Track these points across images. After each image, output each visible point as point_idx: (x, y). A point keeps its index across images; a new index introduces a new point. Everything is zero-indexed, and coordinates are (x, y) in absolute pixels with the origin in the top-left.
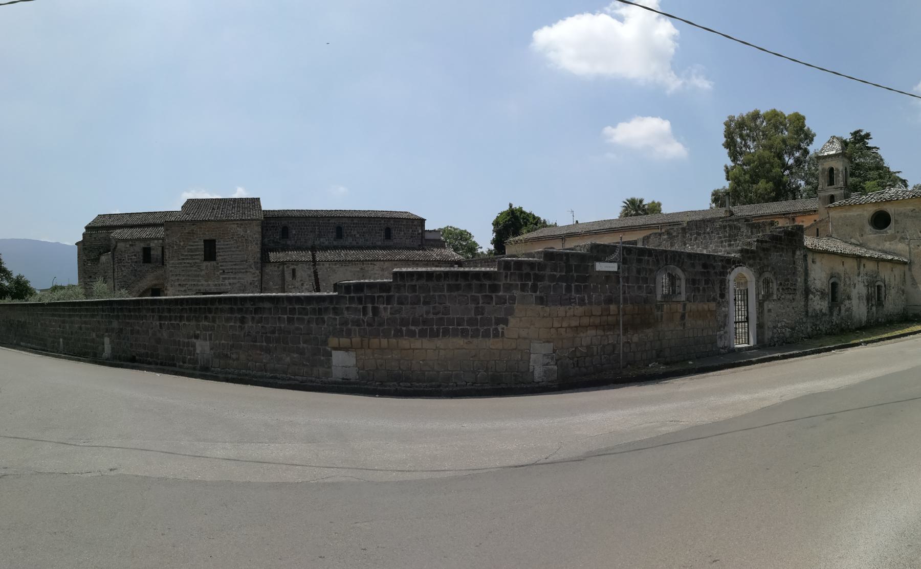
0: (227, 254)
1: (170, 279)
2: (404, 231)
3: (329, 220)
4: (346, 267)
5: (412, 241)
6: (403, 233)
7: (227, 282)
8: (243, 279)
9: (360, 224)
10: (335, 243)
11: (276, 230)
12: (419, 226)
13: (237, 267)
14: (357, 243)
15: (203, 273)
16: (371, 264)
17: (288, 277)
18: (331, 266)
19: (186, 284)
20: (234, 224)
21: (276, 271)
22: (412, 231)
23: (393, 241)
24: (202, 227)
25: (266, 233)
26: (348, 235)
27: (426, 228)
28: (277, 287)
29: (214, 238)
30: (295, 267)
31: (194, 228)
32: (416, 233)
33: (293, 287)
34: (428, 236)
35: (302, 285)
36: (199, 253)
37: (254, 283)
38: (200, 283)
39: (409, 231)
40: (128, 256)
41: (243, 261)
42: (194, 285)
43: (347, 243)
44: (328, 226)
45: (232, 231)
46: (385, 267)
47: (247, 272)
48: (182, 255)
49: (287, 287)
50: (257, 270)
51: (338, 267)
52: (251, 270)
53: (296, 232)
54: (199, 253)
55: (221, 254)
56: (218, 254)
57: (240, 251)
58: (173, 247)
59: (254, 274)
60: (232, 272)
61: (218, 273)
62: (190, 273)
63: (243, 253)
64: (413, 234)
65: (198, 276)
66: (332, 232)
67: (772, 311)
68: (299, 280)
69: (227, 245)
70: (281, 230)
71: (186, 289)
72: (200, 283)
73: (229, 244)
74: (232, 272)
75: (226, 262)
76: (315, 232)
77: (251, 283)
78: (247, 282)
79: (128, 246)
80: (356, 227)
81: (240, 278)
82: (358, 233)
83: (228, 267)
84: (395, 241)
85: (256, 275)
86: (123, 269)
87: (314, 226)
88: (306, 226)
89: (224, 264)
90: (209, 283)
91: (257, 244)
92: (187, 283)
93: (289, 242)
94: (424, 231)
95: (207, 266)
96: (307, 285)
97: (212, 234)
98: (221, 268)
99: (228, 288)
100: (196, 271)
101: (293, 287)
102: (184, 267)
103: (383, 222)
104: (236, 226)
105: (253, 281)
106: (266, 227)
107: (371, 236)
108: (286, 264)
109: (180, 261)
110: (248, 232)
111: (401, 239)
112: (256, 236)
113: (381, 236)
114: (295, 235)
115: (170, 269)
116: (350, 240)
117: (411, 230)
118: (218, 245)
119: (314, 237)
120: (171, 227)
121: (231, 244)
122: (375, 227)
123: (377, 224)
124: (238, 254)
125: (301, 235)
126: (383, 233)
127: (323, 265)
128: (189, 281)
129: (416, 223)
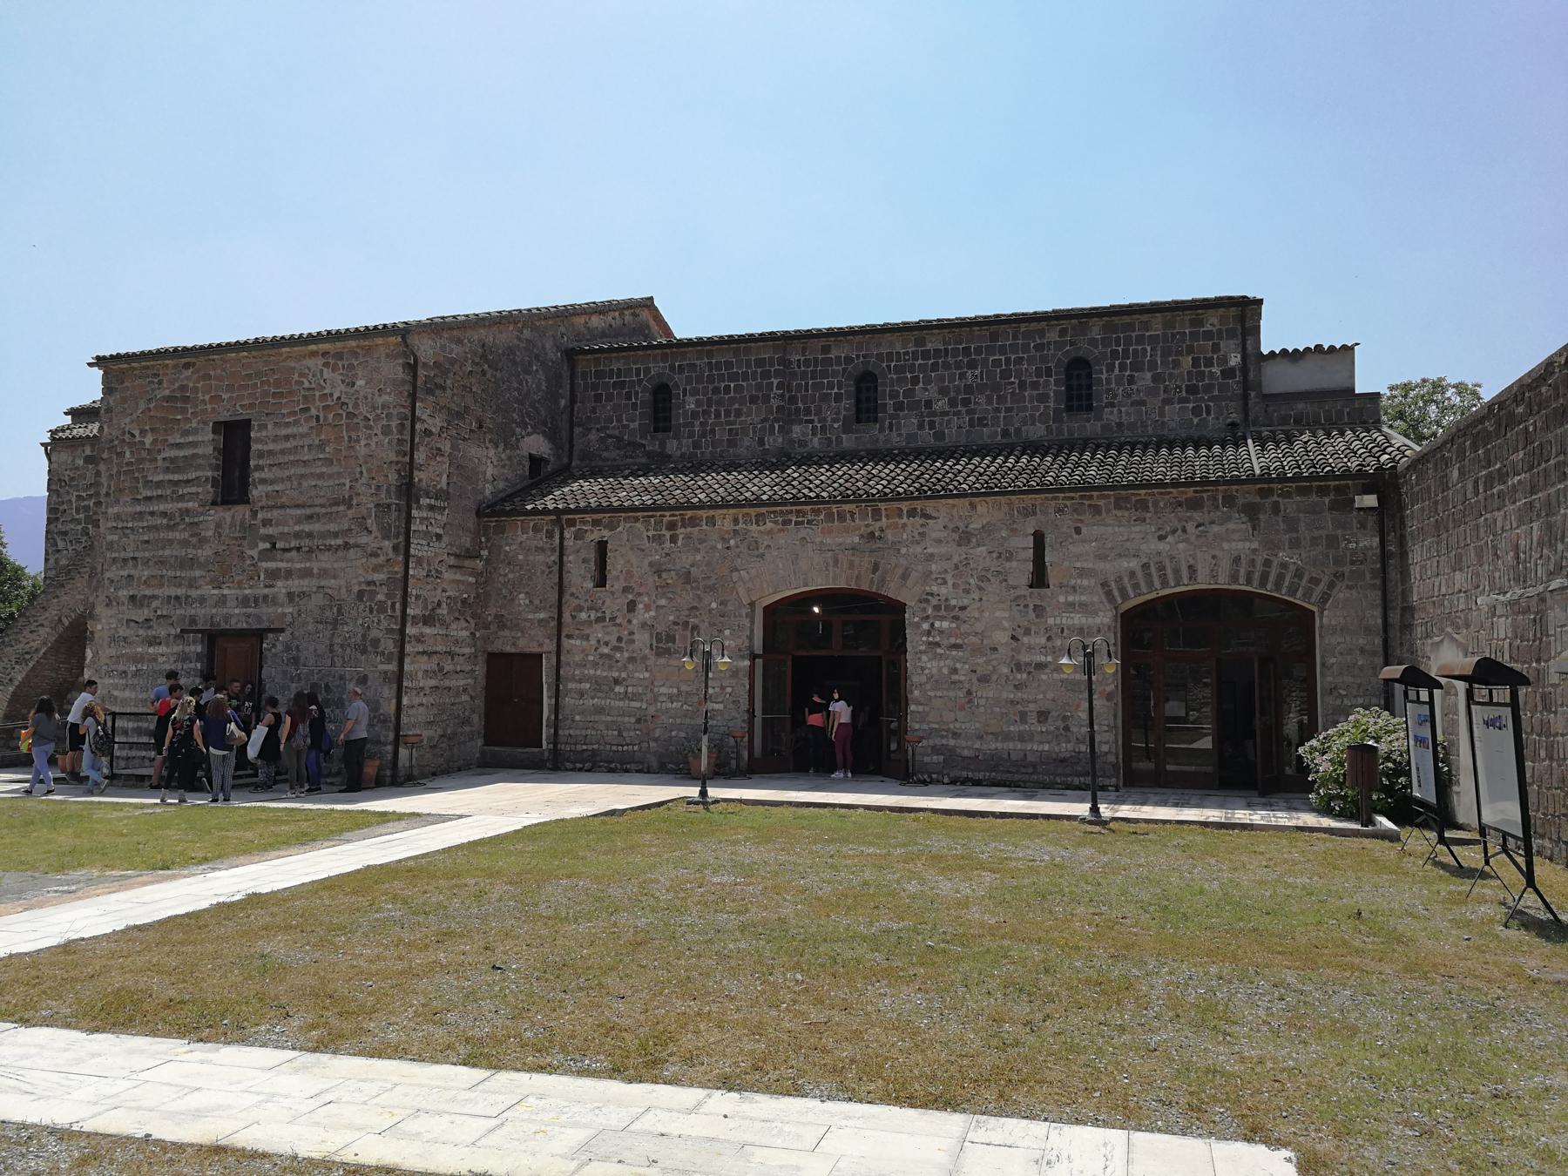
0: (287, 473)
1: (107, 575)
2: (1152, 365)
3: (826, 349)
4: (803, 533)
5: (1196, 411)
6: (1149, 375)
7: (281, 587)
8: (335, 577)
9: (956, 352)
10: (848, 442)
11: (628, 396)
12: (1231, 334)
13: (316, 527)
14: (939, 436)
15: (205, 552)
16: (912, 513)
17: (579, 574)
18: (741, 525)
19: (154, 597)
20: (313, 354)
21: (542, 550)
22: (1196, 363)
23: (1099, 418)
24: (212, 373)
25: (594, 410)
26: (899, 407)
27: (1270, 341)
28: (542, 615)
29: (244, 414)
30: (606, 533)
31: (188, 378)
32: (1216, 370)
33: (593, 615)
34: (1278, 380)
35: (632, 606)
36: (199, 473)
37: (373, 594)
38: (194, 593)
39: (1176, 364)
40: (79, 497)
41: (337, 504)
42: (177, 598)
43: (896, 440)
44: (824, 374)
45: (306, 385)
46: (975, 525)
47: (346, 546)
48: (148, 483)
49: (574, 617)
50: (386, 537)
51: (770, 532)
52: (364, 539)
53: (698, 403)
54: (199, 473)
55: (265, 474)
56: (256, 475)
57: (329, 461)
58: (121, 455)
59: (376, 555)
60: (298, 549)
61: (254, 553)
62: (167, 552)
63: (335, 469)
64: (1201, 375)
65: (191, 563)
66: (838, 398)
67: (227, 515)
68: (618, 586)
69: (287, 438)
70: (647, 396)
71: (151, 615)
72: (194, 593)
73: (294, 436)
74: (298, 549)
75: (283, 507)
76: (767, 399)
77: (361, 594)
78: (349, 591)
79: (80, 462)
80: (935, 367)
81: (324, 573)
82: (943, 391)
83: (286, 530)
84: (1110, 415)
85: (382, 559)
86: (61, 545)
87: (766, 375)
88: (734, 377)
89: (275, 513)
90: (226, 592)
91: (386, 431)
92: (156, 592)
93: (672, 446)
94: (1254, 359)
95: (218, 525)
96: (647, 608)
97: (241, 397)
98: (262, 531)
99: (284, 614)
100: (185, 543)
101: (593, 615)
102: (150, 528)
103: (1053, 336)
104: (320, 361)
105: (369, 583)
106: (595, 387)
107: (1001, 399)
108: (571, 523)
109: (138, 509)
110: (360, 383)
111: (1143, 403)
112: (386, 398)
113: (1043, 398)
114: (695, 414)
115: (110, 538)
116: (909, 423)
117: (1187, 361)
118: (259, 441)
119: (763, 421)
120: (123, 382)
121: (303, 436)
122: (1019, 361)
123: (1026, 348)
124: (321, 476)
125: (718, 415)
126: (1053, 387)
127: (711, 521)
128: (161, 586)
129: (1212, 322)
